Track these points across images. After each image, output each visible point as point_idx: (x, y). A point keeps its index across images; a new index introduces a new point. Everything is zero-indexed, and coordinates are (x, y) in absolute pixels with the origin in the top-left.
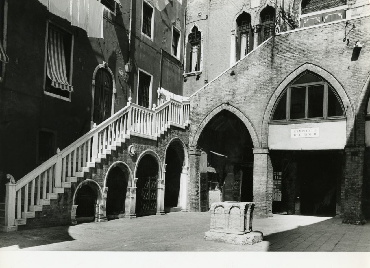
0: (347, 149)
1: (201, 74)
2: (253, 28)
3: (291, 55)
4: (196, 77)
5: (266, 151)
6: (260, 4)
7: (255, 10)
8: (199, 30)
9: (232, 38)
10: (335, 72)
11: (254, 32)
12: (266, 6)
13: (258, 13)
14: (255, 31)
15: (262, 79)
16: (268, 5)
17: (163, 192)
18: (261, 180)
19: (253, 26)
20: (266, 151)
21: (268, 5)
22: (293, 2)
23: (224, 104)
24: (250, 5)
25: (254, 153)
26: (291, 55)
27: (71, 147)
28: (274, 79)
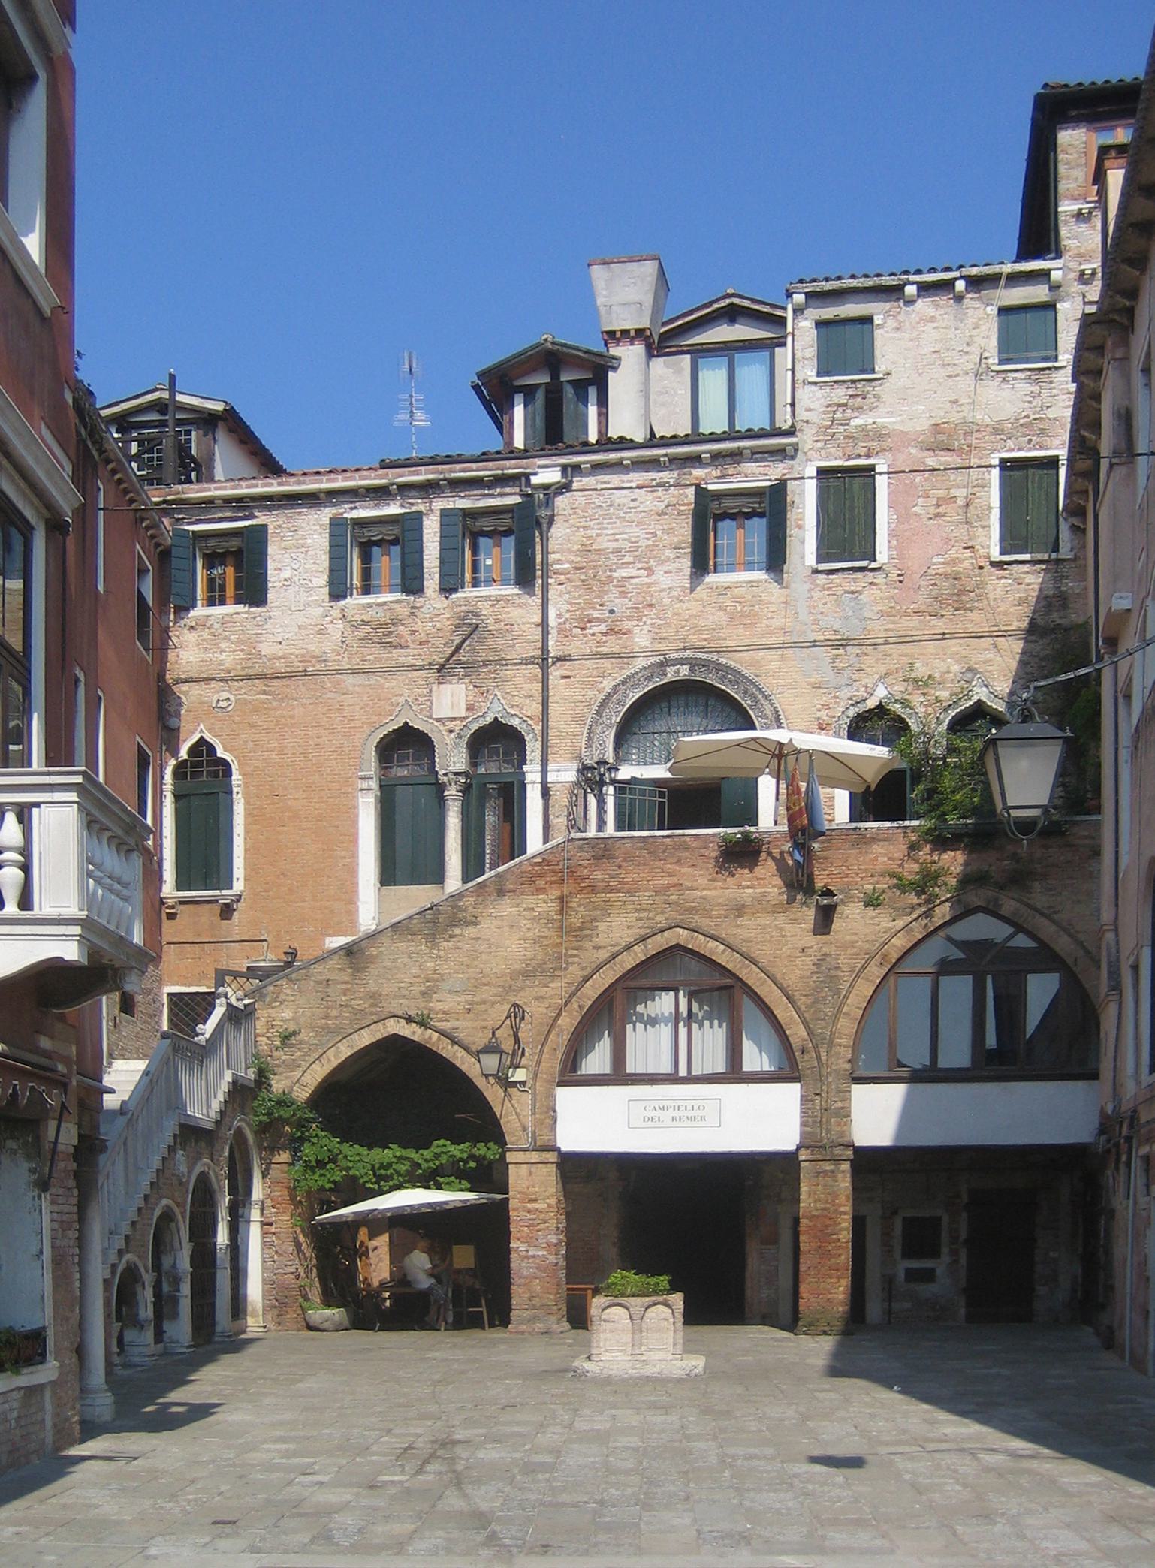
0: (802, 1151)
1: (238, 901)
2: (445, 779)
3: (625, 899)
4: (216, 909)
5: (552, 1157)
6: (467, 709)
7: (450, 725)
8: (219, 755)
9: (360, 799)
10: (763, 955)
11: (446, 793)
12: (489, 719)
13: (459, 736)
14: (452, 791)
15: (529, 957)
16: (496, 718)
17: (189, 1301)
18: (296, 1150)
19: (445, 775)
20: (552, 1157)
21: (496, 718)
22: (587, 727)
23: (392, 1019)
24: (431, 708)
25: (508, 1161)
26: (625, 899)
27: (82, 1272)
28: (571, 960)
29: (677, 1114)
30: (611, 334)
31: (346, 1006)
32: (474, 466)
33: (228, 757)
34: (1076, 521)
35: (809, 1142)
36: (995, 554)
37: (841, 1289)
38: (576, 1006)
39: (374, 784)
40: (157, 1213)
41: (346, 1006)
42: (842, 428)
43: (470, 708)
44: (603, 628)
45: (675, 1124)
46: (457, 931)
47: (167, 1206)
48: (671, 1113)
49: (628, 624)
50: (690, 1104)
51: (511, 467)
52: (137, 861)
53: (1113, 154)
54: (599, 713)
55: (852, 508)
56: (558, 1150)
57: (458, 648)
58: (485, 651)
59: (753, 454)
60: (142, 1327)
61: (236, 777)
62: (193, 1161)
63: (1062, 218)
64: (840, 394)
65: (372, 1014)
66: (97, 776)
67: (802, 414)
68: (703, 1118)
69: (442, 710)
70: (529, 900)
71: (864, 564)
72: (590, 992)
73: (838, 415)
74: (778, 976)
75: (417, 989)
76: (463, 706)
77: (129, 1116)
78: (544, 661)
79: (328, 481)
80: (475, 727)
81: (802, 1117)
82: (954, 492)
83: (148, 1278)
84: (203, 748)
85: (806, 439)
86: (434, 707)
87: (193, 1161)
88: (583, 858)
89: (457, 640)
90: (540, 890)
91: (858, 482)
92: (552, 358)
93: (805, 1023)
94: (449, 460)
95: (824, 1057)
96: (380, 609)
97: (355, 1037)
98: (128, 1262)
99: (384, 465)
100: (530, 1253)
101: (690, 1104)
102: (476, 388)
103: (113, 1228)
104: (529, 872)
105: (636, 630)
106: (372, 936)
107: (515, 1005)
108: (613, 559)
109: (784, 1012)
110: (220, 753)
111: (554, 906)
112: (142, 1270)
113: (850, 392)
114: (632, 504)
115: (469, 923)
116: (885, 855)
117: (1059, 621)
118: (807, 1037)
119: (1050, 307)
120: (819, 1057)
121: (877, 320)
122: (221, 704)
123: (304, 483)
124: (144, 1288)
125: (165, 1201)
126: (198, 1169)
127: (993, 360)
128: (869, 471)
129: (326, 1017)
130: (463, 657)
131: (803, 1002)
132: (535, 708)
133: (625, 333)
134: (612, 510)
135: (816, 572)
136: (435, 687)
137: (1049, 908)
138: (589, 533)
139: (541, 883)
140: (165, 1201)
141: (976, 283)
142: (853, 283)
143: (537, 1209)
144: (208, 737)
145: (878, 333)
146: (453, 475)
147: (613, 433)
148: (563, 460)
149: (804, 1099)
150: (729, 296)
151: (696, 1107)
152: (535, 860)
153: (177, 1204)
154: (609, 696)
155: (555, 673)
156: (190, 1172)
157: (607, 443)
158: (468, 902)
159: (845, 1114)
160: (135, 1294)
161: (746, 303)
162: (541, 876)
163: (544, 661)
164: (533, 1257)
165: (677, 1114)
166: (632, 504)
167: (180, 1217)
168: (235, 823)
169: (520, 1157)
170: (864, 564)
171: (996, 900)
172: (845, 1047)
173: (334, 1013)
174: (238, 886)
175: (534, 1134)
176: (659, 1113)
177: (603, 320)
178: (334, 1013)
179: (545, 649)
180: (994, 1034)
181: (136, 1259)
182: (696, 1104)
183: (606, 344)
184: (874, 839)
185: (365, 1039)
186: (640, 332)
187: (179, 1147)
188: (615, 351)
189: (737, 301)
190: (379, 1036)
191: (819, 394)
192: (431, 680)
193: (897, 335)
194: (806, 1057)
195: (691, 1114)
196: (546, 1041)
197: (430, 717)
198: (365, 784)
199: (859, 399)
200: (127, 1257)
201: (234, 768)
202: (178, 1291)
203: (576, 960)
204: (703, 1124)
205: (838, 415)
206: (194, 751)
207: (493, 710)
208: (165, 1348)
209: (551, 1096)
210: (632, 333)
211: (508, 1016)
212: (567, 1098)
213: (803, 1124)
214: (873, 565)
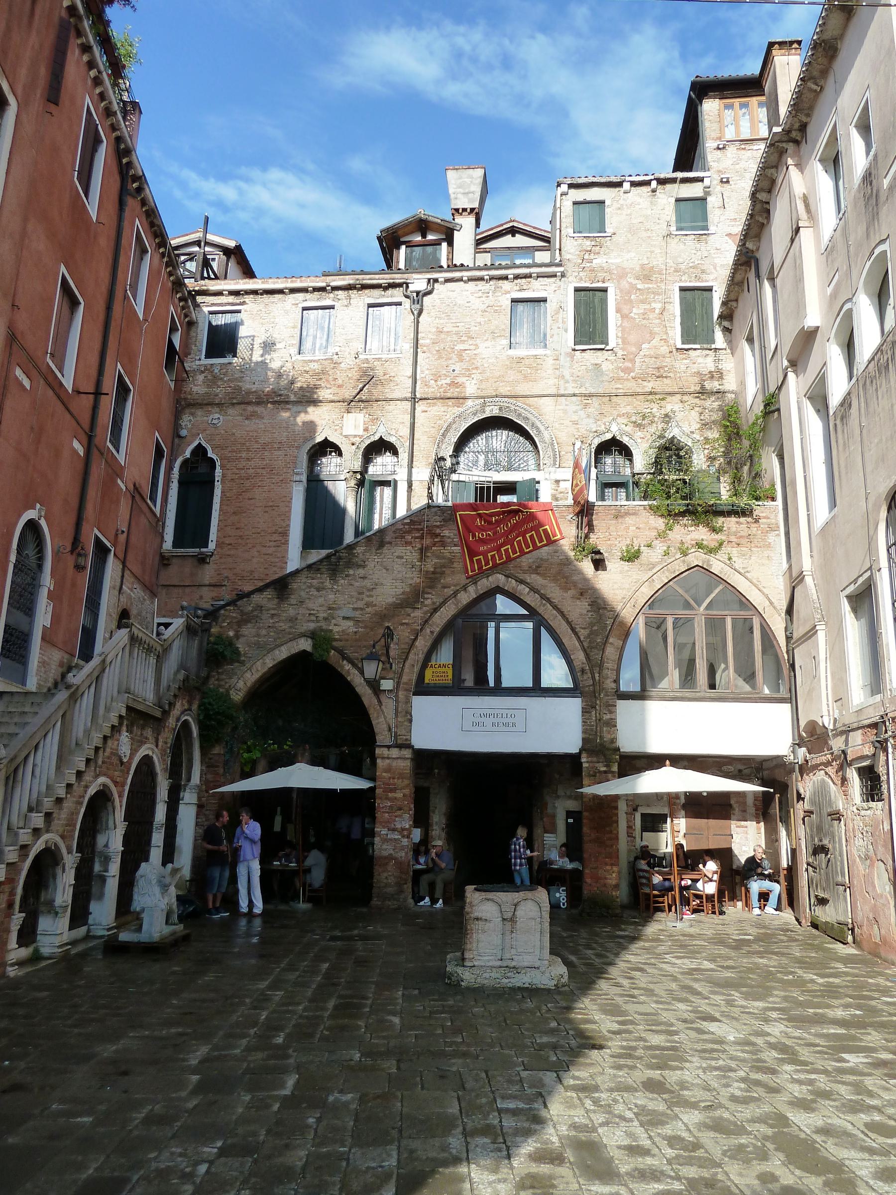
5: (407, 753)
7: (354, 440)
12: (377, 438)
13: (358, 448)
20: (407, 753)
29: (496, 720)
30: (457, 210)
31: (272, 627)
32: (377, 276)
33: (214, 457)
34: (726, 324)
35: (588, 746)
36: (680, 346)
37: (614, 875)
38: (428, 631)
39: (304, 478)
40: (92, 791)
41: (272, 627)
42: (588, 265)
43: (366, 430)
44: (448, 381)
45: (495, 728)
46: (351, 572)
47: (104, 785)
48: (492, 720)
49: (460, 380)
50: (505, 712)
51: (398, 278)
52: (174, 561)
53: (776, 46)
54: (444, 435)
55: (594, 313)
56: (409, 746)
57: (361, 390)
58: (376, 393)
59: (538, 277)
60: (56, 913)
61: (218, 472)
62: (137, 744)
63: (708, 150)
64: (588, 243)
65: (290, 633)
66: (155, 506)
67: (566, 256)
68: (514, 725)
69: (349, 430)
70: (400, 550)
71: (602, 346)
72: (438, 621)
73: (586, 257)
74: (566, 613)
75: (322, 615)
76: (362, 429)
77: (72, 690)
78: (414, 400)
79: (292, 282)
80: (368, 442)
81: (583, 726)
82: (654, 305)
83: (70, 860)
84: (200, 451)
85: (569, 268)
86: (344, 428)
87: (137, 744)
88: (436, 521)
89: (361, 386)
90: (408, 543)
91: (599, 294)
92: (422, 226)
93: (584, 650)
94: (363, 273)
95: (597, 678)
96: (315, 364)
97: (277, 652)
98: (47, 842)
99: (326, 274)
100: (389, 836)
101: (505, 712)
102: (379, 238)
103: (34, 804)
104: (401, 530)
105: (468, 383)
106: (297, 572)
107: (388, 628)
108: (455, 338)
109: (570, 641)
110: (210, 454)
111: (416, 555)
112: (64, 851)
113: (593, 243)
114: (468, 305)
115: (359, 566)
116: (634, 525)
117: (718, 387)
118: (585, 661)
119: (703, 200)
120: (593, 678)
121: (607, 204)
122: (214, 422)
123: (277, 282)
124: (64, 871)
125: (102, 780)
126: (143, 752)
127: (673, 228)
128: (605, 290)
129: (258, 635)
130: (363, 396)
131: (583, 633)
132: (406, 432)
133: (464, 210)
134: (455, 308)
135: (574, 350)
136: (345, 415)
137: (743, 568)
138: (442, 321)
139: (409, 538)
140: (102, 780)
141: (662, 182)
142: (595, 180)
143: (396, 798)
144: (204, 444)
145: (607, 210)
146: (365, 282)
147: (457, 262)
148: (429, 276)
149: (585, 711)
150: (511, 221)
151: (505, 716)
152: (406, 521)
153: (116, 783)
154: (449, 426)
155: (420, 407)
156: (133, 752)
157: (453, 267)
158: (359, 550)
159: (612, 724)
160: (54, 877)
161: (521, 226)
162: (409, 532)
163: (414, 400)
164: (391, 840)
165: (496, 720)
166: (468, 305)
167: (116, 795)
168: (214, 502)
169: (385, 752)
170: (602, 346)
171: (709, 561)
172: (612, 670)
173: (264, 632)
174: (212, 546)
175: (396, 733)
176: (483, 719)
177: (453, 202)
178: (264, 632)
179: (414, 391)
180: (760, 643)
181: (58, 839)
182: (510, 712)
183: (453, 214)
184: (627, 514)
185: (283, 653)
186: (472, 210)
187: (124, 728)
188: (459, 220)
189: (515, 224)
190: (293, 651)
191: (576, 243)
192: (343, 410)
193: (619, 212)
194: (585, 677)
195: (505, 720)
196: (407, 658)
197: (341, 434)
198: (297, 478)
199: (598, 248)
200: (45, 837)
201: (218, 464)
202: (106, 871)
203: (430, 596)
204: (514, 729)
205: (586, 257)
206: (194, 452)
207: (380, 432)
208: (89, 931)
209: (408, 702)
210: (469, 210)
211: (384, 635)
212: (421, 705)
213: (584, 732)
214: (608, 348)
